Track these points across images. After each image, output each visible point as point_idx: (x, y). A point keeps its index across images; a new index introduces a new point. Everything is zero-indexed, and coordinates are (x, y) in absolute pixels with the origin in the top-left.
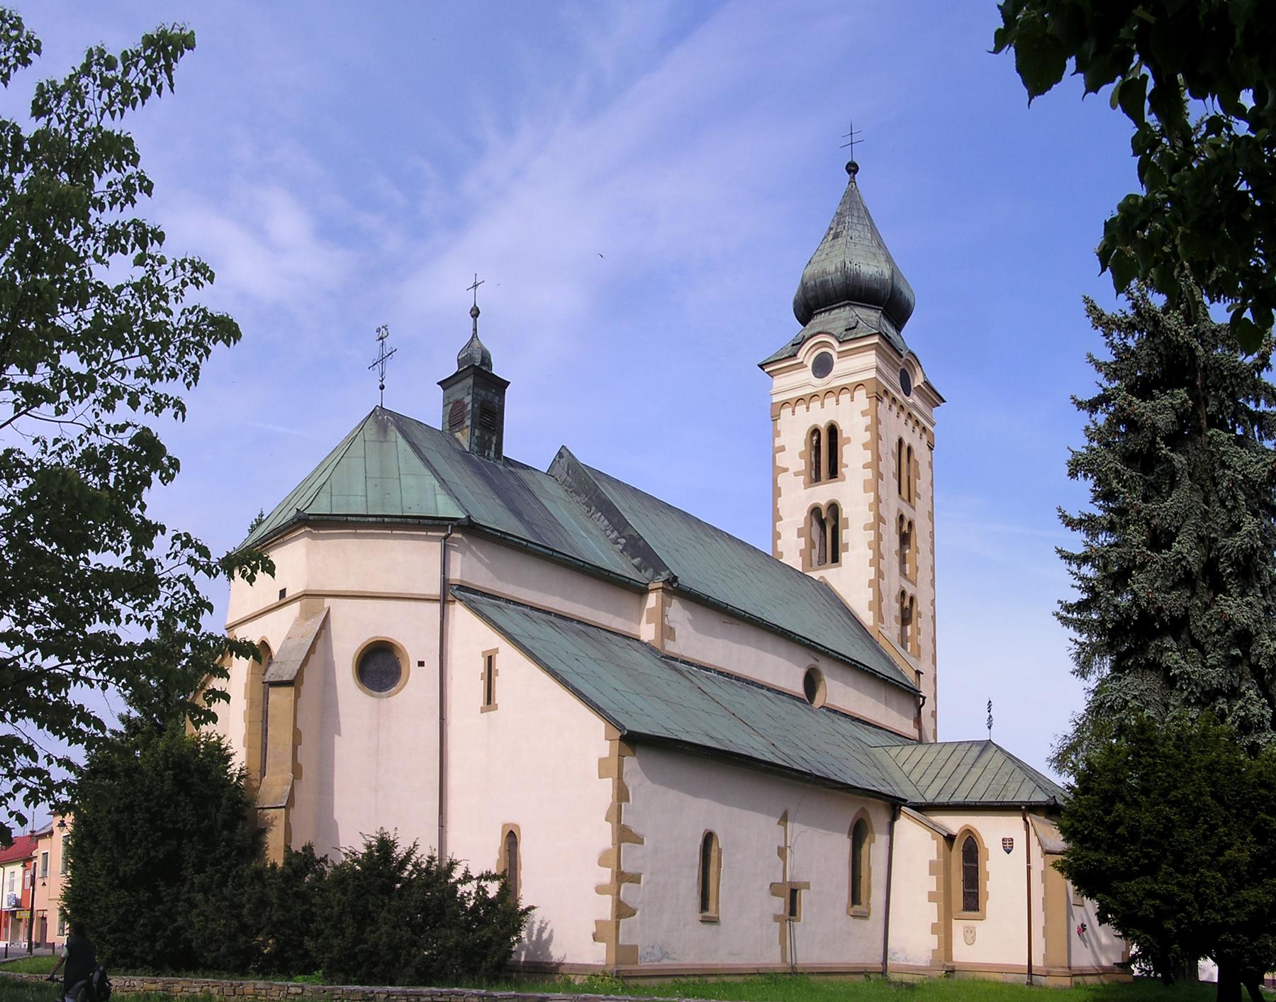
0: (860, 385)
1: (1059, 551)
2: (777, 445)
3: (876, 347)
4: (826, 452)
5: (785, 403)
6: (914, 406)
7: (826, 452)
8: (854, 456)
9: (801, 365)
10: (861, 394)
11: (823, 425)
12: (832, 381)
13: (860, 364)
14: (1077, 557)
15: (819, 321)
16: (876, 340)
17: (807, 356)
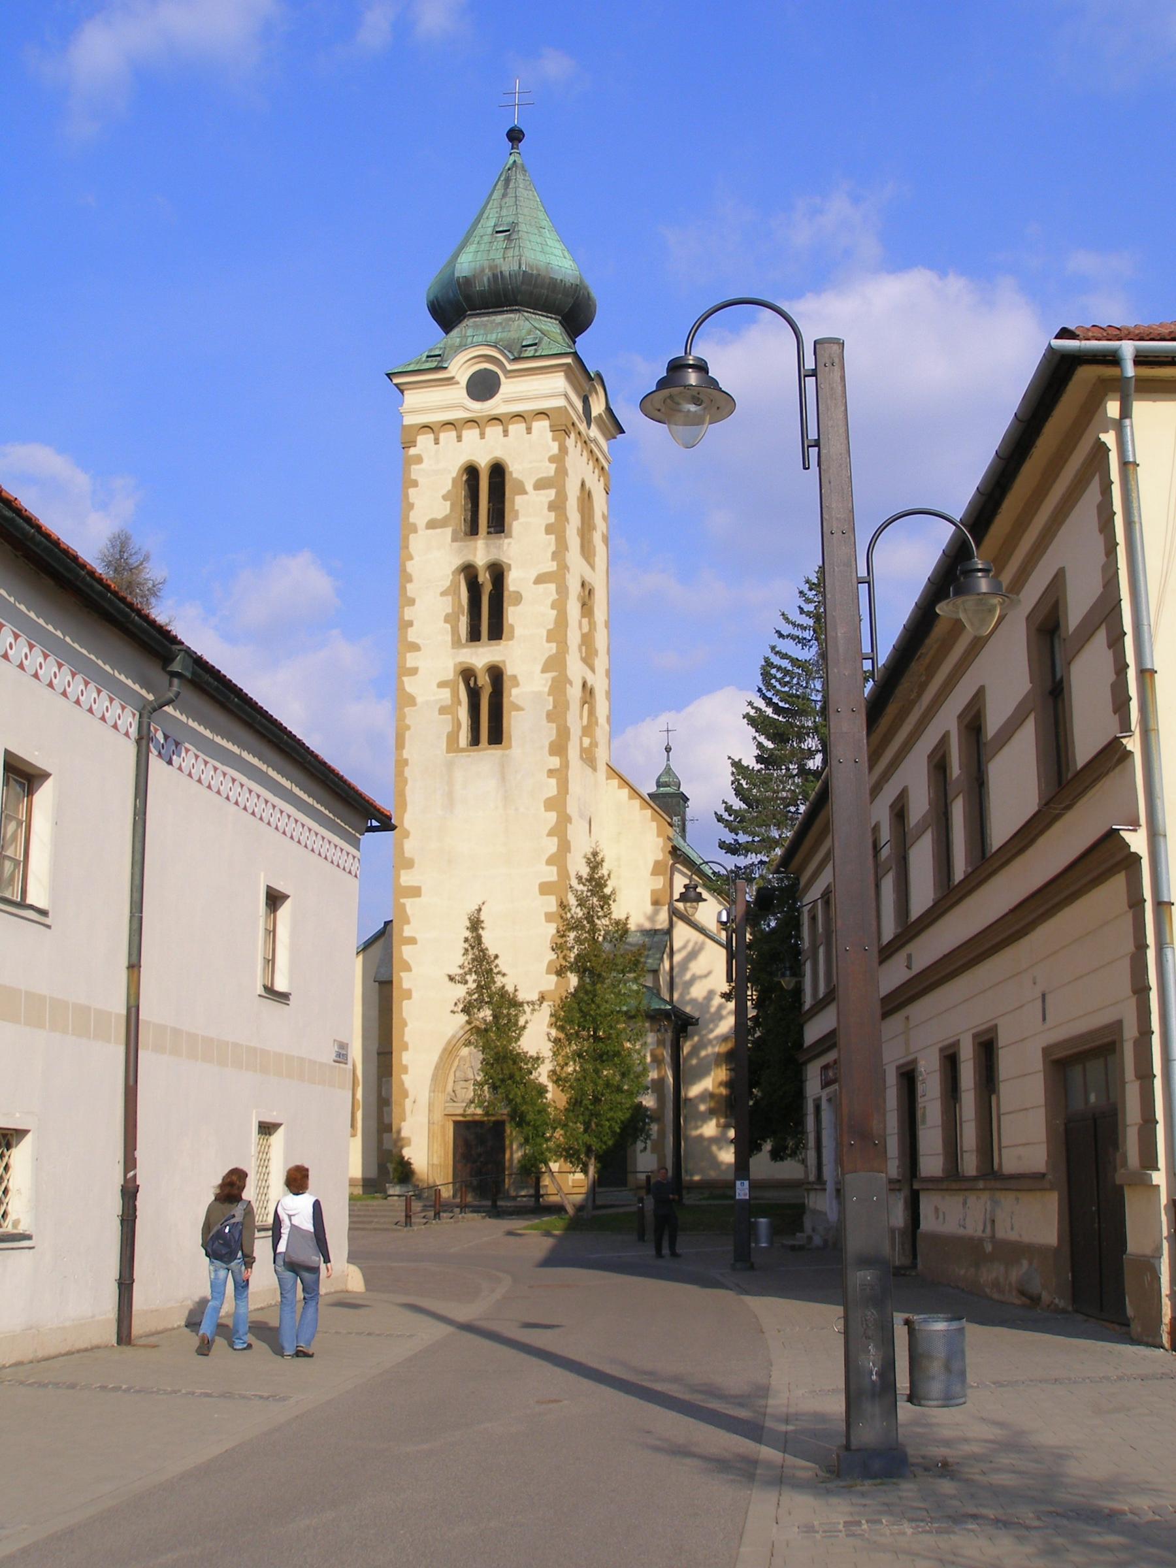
0: (543, 414)
1: (475, 925)
2: (552, 587)
3: (567, 369)
4: (486, 497)
6: (595, 441)
7: (486, 497)
8: (529, 511)
9: (450, 381)
10: (542, 427)
11: (483, 463)
12: (495, 405)
13: (549, 388)
14: (479, 939)
15: (469, 327)
16: (569, 360)
17: (461, 368)
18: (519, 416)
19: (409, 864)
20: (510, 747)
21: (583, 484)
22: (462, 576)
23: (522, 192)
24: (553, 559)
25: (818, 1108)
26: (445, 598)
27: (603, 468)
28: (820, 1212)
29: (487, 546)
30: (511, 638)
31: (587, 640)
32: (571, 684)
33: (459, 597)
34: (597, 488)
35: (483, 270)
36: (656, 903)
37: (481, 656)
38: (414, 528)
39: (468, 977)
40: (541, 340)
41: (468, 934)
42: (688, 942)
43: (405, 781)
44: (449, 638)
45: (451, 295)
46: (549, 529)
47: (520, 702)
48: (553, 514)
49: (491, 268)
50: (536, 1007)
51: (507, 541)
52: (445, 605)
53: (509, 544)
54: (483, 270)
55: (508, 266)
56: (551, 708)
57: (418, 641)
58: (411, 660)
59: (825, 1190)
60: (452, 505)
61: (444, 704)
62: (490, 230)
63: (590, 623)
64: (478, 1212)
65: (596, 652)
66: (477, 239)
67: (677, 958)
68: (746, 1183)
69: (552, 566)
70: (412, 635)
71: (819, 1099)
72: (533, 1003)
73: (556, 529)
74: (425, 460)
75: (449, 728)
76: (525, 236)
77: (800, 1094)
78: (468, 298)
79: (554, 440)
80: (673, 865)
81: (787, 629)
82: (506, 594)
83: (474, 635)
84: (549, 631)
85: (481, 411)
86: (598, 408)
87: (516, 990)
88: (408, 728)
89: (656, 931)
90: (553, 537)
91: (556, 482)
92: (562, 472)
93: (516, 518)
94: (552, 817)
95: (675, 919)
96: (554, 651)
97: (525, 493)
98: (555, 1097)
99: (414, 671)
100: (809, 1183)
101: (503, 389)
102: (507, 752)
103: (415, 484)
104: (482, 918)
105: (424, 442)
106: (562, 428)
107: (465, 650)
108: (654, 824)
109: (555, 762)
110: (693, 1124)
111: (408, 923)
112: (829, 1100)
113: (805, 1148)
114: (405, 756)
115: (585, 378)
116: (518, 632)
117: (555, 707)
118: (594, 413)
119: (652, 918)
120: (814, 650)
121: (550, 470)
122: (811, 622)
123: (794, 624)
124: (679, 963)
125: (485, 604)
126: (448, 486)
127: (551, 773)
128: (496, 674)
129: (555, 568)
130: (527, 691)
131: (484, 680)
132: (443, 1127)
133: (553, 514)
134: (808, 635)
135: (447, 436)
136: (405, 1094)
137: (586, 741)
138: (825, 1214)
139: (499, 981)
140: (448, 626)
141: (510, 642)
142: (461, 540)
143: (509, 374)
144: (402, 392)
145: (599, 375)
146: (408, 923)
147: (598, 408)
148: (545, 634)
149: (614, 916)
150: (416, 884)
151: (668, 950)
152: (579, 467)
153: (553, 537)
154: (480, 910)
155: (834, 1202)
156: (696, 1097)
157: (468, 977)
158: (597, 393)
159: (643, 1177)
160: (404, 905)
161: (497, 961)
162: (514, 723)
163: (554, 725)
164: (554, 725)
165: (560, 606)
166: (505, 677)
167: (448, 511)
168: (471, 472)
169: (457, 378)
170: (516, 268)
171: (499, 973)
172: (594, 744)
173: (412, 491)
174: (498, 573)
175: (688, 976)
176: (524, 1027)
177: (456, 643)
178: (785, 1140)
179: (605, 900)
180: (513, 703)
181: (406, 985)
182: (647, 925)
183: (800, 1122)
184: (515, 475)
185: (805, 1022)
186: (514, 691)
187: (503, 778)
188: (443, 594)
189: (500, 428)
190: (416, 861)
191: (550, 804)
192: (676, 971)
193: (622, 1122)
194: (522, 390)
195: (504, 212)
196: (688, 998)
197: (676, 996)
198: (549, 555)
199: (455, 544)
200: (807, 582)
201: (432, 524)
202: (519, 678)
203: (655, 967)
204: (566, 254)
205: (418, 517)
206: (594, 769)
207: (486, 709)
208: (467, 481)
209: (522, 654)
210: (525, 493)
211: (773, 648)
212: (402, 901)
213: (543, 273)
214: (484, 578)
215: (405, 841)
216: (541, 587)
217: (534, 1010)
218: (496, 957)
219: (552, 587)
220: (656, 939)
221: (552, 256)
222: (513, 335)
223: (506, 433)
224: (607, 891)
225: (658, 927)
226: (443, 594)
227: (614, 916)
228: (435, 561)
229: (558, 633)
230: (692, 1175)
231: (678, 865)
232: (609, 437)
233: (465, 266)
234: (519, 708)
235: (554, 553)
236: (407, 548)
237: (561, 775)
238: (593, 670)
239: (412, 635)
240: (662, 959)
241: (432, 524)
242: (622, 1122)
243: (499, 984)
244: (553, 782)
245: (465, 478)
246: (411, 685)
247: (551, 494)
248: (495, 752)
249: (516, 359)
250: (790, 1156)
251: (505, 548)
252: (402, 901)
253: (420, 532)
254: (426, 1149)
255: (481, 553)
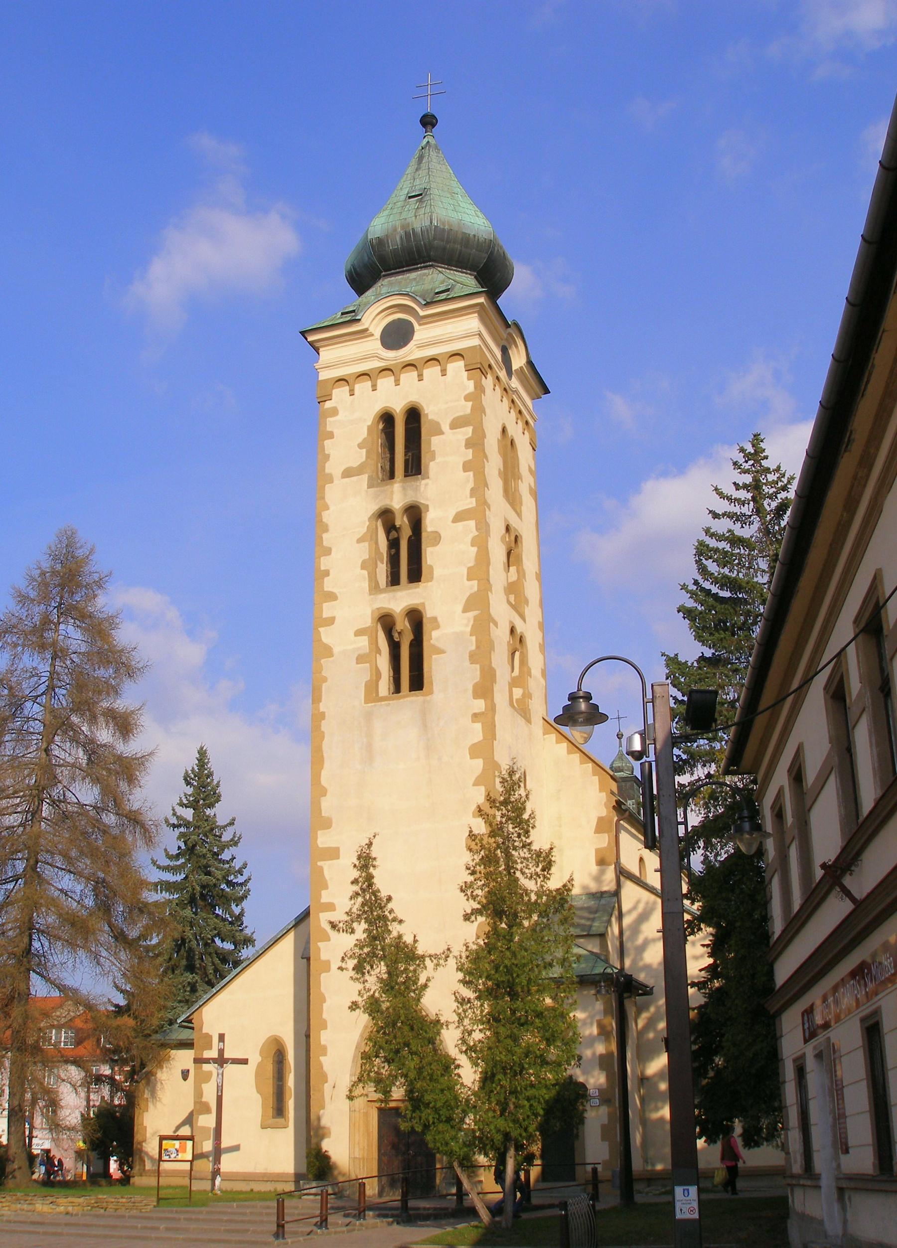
0: (457, 355)
2: (472, 524)
4: (403, 441)
5: (342, 380)
6: (516, 392)
7: (403, 441)
8: (445, 451)
9: (364, 333)
10: (457, 367)
11: (398, 408)
13: (465, 329)
14: (369, 878)
15: (384, 285)
18: (433, 359)
19: (327, 824)
20: (431, 692)
21: (504, 430)
22: (380, 523)
23: (434, 164)
24: (471, 497)
25: (801, 1071)
26: (362, 544)
27: (527, 423)
28: (812, 1219)
29: (404, 489)
30: (431, 579)
31: (514, 589)
32: (496, 624)
33: (377, 543)
34: (516, 430)
35: (395, 230)
36: (601, 862)
37: (399, 601)
38: (330, 479)
39: (355, 925)
40: (453, 286)
41: (356, 874)
42: (638, 902)
43: (322, 736)
44: (366, 585)
45: (366, 258)
46: (467, 467)
47: (441, 645)
48: (470, 451)
49: (403, 227)
50: (442, 962)
51: (423, 482)
52: (363, 552)
53: (426, 485)
54: (395, 230)
55: (419, 223)
56: (474, 648)
57: (335, 590)
58: (328, 610)
59: (818, 1187)
60: (367, 452)
61: (361, 652)
62: (403, 198)
63: (518, 572)
64: (386, 1216)
65: (527, 602)
66: (390, 206)
67: (627, 921)
68: (693, 1190)
69: (471, 503)
70: (329, 585)
71: (803, 1056)
72: (436, 956)
73: (475, 466)
74: (341, 412)
75: (367, 677)
76: (437, 198)
77: (774, 1056)
78: (382, 259)
79: (469, 379)
80: (618, 821)
81: (723, 506)
82: (424, 535)
83: (394, 580)
84: (469, 569)
85: (395, 359)
86: (518, 360)
87: (415, 941)
88: (325, 680)
89: (602, 894)
90: (471, 474)
91: (474, 419)
92: (479, 410)
93: (433, 458)
94: (479, 763)
95: (622, 878)
96: (476, 589)
97: (443, 433)
98: (469, 1075)
99: (331, 621)
100: (793, 1176)
101: (417, 336)
102: (428, 698)
103: (331, 435)
104: (373, 855)
105: (340, 394)
106: (479, 368)
107: (383, 595)
108: (596, 779)
109: (480, 705)
110: (652, 1106)
111: (326, 887)
112: (819, 1056)
113: (785, 1128)
114: (322, 710)
115: (505, 328)
116: (437, 572)
117: (478, 647)
118: (515, 367)
119: (598, 879)
120: (756, 525)
121: (467, 408)
122: (749, 496)
123: (729, 499)
124: (629, 926)
125: (404, 549)
126: (364, 433)
127: (476, 717)
128: (416, 618)
129: (474, 505)
130: (446, 664)
131: (403, 625)
132: (366, 1115)
133: (470, 451)
134: (747, 510)
135: (362, 387)
136: (324, 1078)
137: (518, 693)
138: (821, 1222)
139: (395, 929)
140: (365, 573)
141: (430, 583)
142: (378, 486)
143: (422, 320)
144: (317, 350)
145: (516, 325)
146: (326, 887)
147: (518, 360)
148: (465, 572)
149: (535, 847)
150: (334, 845)
151: (616, 912)
152: (498, 413)
153: (471, 474)
154: (370, 845)
155: (836, 1207)
156: (655, 1075)
157: (355, 925)
158: (516, 346)
159: (589, 1168)
160: (321, 868)
161: (390, 906)
162: (436, 667)
163: (478, 666)
164: (478, 666)
165: (481, 543)
166: (425, 621)
167: (364, 459)
168: (387, 419)
169: (371, 330)
170: (428, 223)
171: (394, 920)
172: (527, 695)
173: (327, 443)
174: (415, 514)
175: (640, 940)
176: (425, 986)
177: (375, 588)
178: (758, 1119)
179: (525, 827)
180: (433, 646)
181: (324, 957)
182: (593, 887)
183: (776, 1108)
184: (430, 417)
185: (776, 959)
186: (435, 634)
187: (425, 725)
188: (359, 541)
189: (415, 374)
190: (334, 820)
191: (475, 751)
192: (626, 934)
193: (547, 1102)
194: (435, 335)
195: (417, 182)
196: (641, 964)
197: (627, 963)
198: (468, 492)
199: (372, 490)
200: (742, 450)
201: (348, 473)
202: (439, 619)
203: (602, 930)
204: (479, 214)
205: (335, 467)
206: (529, 721)
207: (407, 656)
208: (383, 430)
209: (443, 597)
210: (443, 433)
211: (707, 531)
212: (319, 863)
213: (455, 228)
214: (402, 521)
215: (323, 799)
216: (460, 525)
217: (438, 965)
218: (389, 899)
219: (472, 524)
220: (603, 901)
221: (463, 213)
222: (427, 286)
223: (420, 378)
224: (526, 816)
225: (605, 888)
226: (359, 541)
227: (535, 847)
228: (350, 510)
229: (479, 570)
230: (653, 1165)
231: (622, 822)
232: (535, 397)
233: (378, 228)
234: (441, 652)
235: (472, 490)
236: (323, 498)
237: (487, 719)
238: (523, 618)
239: (329, 585)
240: (609, 922)
241: (348, 473)
242: (547, 1102)
243: (395, 934)
244: (478, 726)
245: (381, 426)
246: (327, 635)
247: (468, 431)
248: (416, 699)
249: (428, 304)
250: (767, 1140)
251: (422, 489)
252: (319, 863)
253: (336, 482)
254: (350, 1144)
255: (397, 497)
